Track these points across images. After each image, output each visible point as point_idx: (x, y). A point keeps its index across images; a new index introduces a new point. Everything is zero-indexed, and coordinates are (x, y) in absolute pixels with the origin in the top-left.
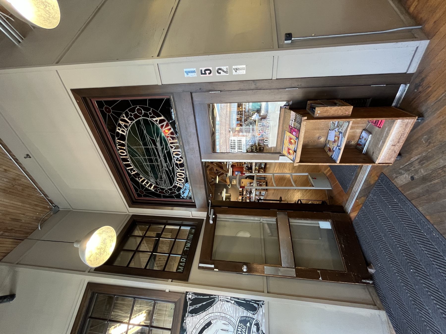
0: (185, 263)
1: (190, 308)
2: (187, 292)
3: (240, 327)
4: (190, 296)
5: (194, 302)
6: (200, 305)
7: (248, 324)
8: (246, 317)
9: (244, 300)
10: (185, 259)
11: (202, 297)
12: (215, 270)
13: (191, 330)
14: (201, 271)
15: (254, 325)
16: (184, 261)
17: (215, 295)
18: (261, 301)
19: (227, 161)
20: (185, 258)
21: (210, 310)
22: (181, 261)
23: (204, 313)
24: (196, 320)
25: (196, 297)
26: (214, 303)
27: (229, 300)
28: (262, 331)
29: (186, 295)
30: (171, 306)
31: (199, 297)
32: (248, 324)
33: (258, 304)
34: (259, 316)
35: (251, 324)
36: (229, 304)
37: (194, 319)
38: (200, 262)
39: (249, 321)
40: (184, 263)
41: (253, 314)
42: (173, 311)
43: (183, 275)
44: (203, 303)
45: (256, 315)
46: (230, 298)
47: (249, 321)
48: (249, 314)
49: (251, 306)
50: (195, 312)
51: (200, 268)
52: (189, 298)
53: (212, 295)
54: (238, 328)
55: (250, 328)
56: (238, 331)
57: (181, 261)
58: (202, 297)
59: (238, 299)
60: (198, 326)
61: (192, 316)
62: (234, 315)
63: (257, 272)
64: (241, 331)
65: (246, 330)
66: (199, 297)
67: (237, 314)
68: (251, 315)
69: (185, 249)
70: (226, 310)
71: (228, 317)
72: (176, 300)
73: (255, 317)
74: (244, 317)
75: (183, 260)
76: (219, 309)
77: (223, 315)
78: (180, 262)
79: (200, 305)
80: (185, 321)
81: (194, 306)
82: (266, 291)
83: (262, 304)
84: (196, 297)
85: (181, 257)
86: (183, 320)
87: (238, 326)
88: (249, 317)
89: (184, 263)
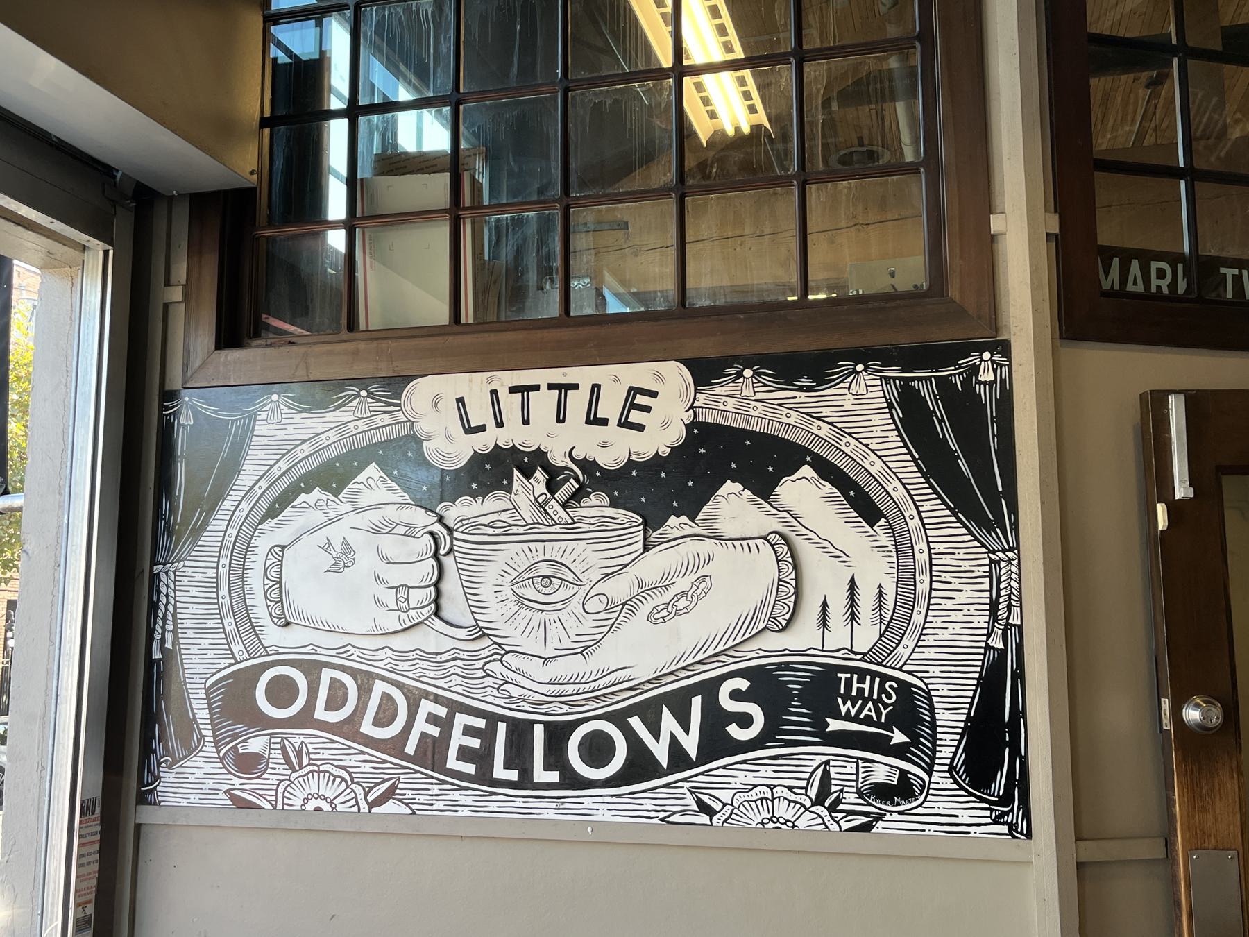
0: (1146, 296)
1: (925, 381)
2: (1004, 348)
3: (882, 690)
4: (987, 375)
5: (962, 402)
6: (953, 445)
7: (898, 737)
8: (933, 726)
9: (1019, 713)
10: (1164, 284)
11: (993, 444)
12: (1161, 509)
13: (826, 412)
14: (1132, 414)
15: (903, 773)
16: (1155, 282)
17: (1015, 527)
18: (1027, 816)
19: (516, 803)
20: (1173, 285)
21: (934, 508)
22: (1155, 265)
23: (912, 473)
24: (878, 432)
25: (991, 411)
26: (973, 526)
27: (1002, 614)
28: (880, 818)
29: (992, 348)
30: (910, 270)
31: (993, 429)
32: (898, 737)
33: (1006, 799)
34: (946, 803)
35: (899, 752)
36: (982, 621)
37: (876, 420)
38: (1196, 403)
39: (915, 739)
40: (1140, 288)
41: (951, 768)
42: (881, 284)
43: (1089, 308)
44: (963, 458)
45: (948, 783)
46: (1015, 621)
47: (915, 739)
48: (948, 745)
49: (990, 747)
50: (913, 418)
51: (1155, 403)
52: (974, 370)
53: (1013, 509)
54: (874, 675)
55: (880, 745)
56: (862, 674)
57: (1155, 265)
58: (993, 444)
59: (1019, 674)
60: (850, 446)
61: (890, 406)
62: (932, 653)
63: (1195, 798)
64: (860, 691)
65: (868, 721)
66: (993, 429)
67: (936, 671)
68: (945, 753)
69: (1230, 272)
70: (949, 604)
71: (918, 619)
72: (954, 292)
73: (941, 779)
74: (932, 710)
75: (1161, 274)
76: (946, 560)
77: (923, 587)
78: (1145, 257)
79: (953, 445)
80: (860, 367)
81: (938, 409)
82: (1091, 852)
83: (1011, 827)
84: (991, 411)
85: (1174, 259)
86: (863, 356)
87: (885, 678)
88: (933, 738)
89: (1140, 288)
